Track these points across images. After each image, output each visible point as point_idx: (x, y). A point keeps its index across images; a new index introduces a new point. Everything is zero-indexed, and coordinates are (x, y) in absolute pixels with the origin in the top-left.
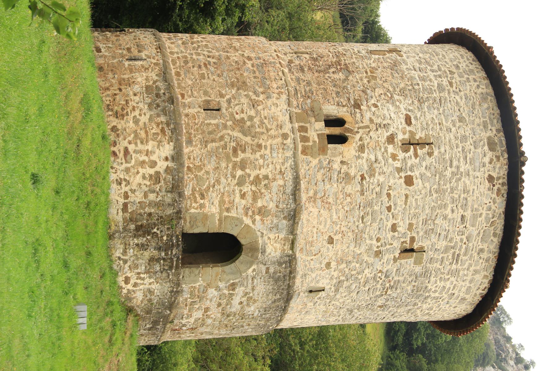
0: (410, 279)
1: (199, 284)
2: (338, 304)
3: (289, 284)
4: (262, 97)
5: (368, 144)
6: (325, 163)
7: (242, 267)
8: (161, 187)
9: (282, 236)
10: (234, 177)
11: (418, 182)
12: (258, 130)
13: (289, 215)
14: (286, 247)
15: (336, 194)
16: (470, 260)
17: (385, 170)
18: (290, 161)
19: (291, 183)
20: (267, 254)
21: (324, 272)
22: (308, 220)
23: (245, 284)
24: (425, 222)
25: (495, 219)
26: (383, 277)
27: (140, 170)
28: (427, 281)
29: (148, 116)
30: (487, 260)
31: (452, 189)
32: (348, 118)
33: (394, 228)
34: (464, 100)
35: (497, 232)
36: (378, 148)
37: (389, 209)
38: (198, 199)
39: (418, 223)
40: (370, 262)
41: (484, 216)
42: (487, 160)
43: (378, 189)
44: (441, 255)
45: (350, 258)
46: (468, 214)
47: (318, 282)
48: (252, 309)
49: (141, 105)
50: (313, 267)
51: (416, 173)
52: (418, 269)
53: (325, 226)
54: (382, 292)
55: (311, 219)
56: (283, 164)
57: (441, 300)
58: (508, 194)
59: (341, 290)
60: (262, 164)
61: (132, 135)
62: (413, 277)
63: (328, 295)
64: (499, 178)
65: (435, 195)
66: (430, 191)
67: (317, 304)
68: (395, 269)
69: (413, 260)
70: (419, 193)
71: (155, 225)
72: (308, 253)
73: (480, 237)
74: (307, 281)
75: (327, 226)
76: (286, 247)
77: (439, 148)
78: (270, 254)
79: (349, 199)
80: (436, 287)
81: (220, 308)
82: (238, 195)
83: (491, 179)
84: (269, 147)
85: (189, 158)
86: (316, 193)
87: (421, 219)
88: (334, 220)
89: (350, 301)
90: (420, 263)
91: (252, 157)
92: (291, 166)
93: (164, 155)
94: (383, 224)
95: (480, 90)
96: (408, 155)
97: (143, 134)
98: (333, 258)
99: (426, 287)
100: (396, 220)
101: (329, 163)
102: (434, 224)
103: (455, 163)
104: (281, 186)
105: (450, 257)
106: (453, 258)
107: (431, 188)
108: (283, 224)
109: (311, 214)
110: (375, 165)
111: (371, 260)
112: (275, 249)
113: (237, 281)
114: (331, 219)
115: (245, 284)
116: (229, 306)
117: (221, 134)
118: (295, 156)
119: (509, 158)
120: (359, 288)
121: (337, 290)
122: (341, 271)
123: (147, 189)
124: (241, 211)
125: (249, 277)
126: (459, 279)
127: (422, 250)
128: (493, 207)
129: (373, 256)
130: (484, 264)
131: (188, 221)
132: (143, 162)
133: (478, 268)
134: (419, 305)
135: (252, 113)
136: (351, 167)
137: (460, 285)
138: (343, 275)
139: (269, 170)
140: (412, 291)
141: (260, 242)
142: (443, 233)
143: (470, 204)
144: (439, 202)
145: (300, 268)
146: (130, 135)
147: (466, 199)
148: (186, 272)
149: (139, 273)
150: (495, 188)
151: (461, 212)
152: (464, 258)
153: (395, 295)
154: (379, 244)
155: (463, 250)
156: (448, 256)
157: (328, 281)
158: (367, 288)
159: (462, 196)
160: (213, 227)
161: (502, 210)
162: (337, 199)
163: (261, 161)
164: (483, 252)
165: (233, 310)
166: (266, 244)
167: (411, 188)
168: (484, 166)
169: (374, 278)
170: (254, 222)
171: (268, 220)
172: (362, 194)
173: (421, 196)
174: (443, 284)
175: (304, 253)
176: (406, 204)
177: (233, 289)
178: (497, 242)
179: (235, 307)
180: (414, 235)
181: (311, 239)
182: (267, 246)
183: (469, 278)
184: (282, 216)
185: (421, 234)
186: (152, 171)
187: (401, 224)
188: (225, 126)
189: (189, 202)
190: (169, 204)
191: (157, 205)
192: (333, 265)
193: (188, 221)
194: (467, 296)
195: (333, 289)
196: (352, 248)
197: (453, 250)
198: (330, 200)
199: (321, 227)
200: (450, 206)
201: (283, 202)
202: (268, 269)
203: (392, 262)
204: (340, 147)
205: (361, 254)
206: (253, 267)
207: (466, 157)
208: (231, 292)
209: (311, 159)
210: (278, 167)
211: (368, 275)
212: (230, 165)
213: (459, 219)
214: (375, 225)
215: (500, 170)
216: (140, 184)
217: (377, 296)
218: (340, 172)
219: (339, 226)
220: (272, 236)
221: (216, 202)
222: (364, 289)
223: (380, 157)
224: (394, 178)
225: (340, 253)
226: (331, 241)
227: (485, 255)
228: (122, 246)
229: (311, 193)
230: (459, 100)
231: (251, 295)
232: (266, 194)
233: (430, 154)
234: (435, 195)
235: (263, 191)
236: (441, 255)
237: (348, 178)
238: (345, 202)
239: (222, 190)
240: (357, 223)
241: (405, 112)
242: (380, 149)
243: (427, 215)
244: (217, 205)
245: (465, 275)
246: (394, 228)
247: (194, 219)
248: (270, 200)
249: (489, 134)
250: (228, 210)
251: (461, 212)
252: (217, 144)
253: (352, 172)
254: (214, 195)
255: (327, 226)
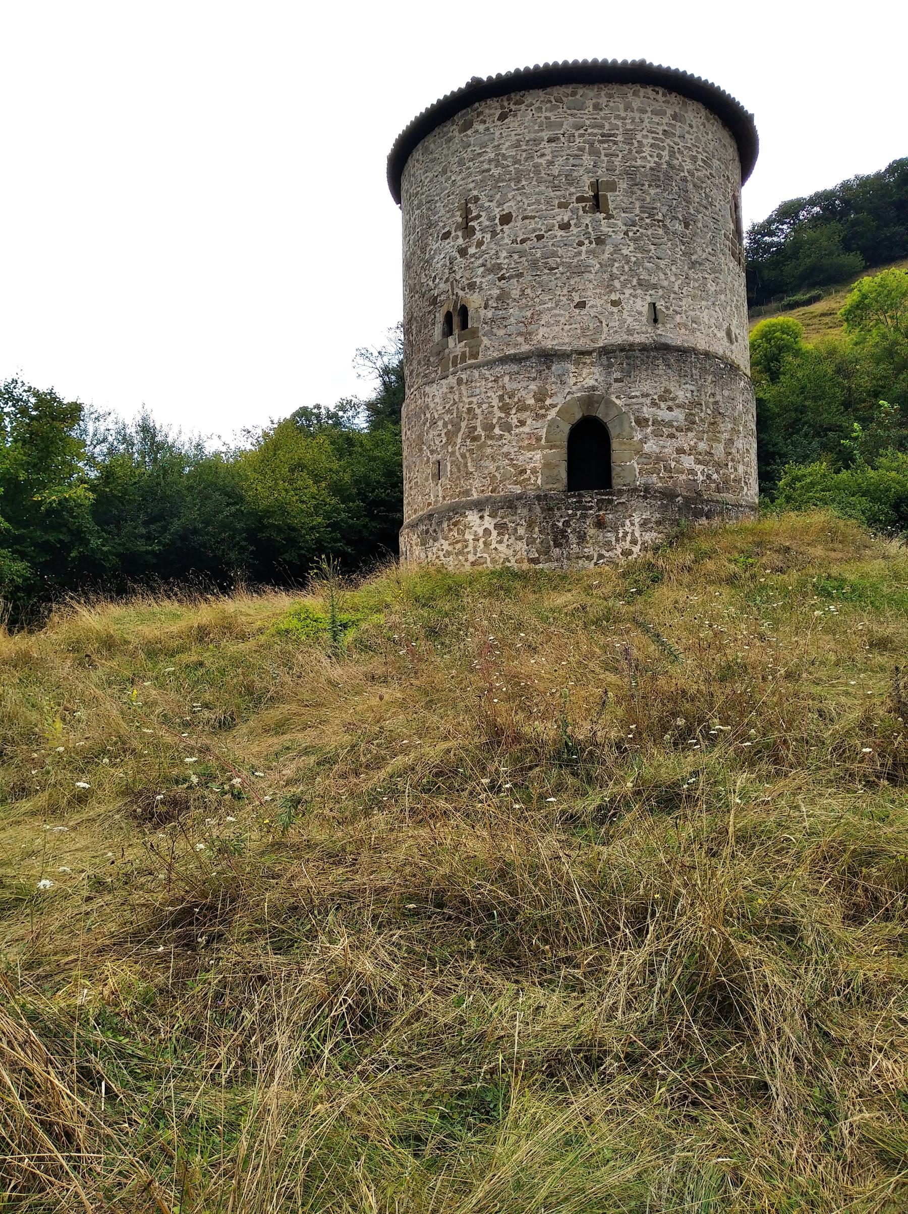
0: (639, 192)
1: (635, 465)
2: (680, 281)
3: (640, 350)
4: (428, 415)
5: (468, 279)
6: (487, 328)
7: (613, 412)
8: (510, 522)
9: (572, 368)
10: (501, 436)
11: (508, 207)
12: (455, 415)
13: (545, 363)
14: (588, 361)
15: (521, 309)
16: (609, 118)
17: (494, 252)
18: (483, 371)
19: (507, 366)
20: (596, 384)
21: (625, 306)
22: (554, 338)
23: (636, 407)
24: (556, 188)
25: (552, 99)
26: (635, 229)
27: (492, 547)
28: (643, 170)
29: (443, 541)
30: (611, 96)
31: (515, 163)
32: (444, 310)
33: (565, 227)
34: (428, 174)
35: (569, 93)
36: (471, 266)
37: (540, 238)
38: (526, 476)
39: (558, 197)
40: (612, 249)
41: (548, 114)
42: (481, 128)
43: (516, 256)
44: (603, 157)
45: (606, 276)
46: (546, 135)
47: (640, 313)
48: (682, 394)
49: (435, 549)
50: (617, 323)
51: (497, 212)
52: (623, 185)
53: (561, 315)
54: (659, 226)
55: (549, 336)
56: (487, 379)
57: (676, 147)
58: (520, 91)
59: (654, 281)
60: (487, 405)
61: (460, 557)
62: (635, 188)
63: (662, 297)
64: (502, 107)
65: (524, 183)
66: (518, 189)
67: (678, 309)
68: (623, 215)
69: (609, 194)
70: (521, 204)
71: (554, 525)
72: (598, 330)
73: (576, 111)
74: (637, 327)
75: (562, 312)
76: (588, 361)
77: (471, 190)
78: (596, 380)
79: (528, 291)
80: (651, 156)
81: (678, 434)
82: (521, 429)
83: (503, 117)
84: (470, 399)
85: (483, 491)
86: (520, 334)
87: (552, 194)
88: (554, 305)
89: (673, 268)
90: (614, 183)
91: (480, 418)
92: (489, 370)
93: (478, 521)
94: (559, 241)
95: (421, 158)
96: (478, 228)
97: (459, 546)
98: (606, 298)
99: (651, 169)
100: (554, 226)
101: (486, 323)
102: (559, 175)
103: (486, 166)
104: (511, 378)
105: (606, 146)
106: (607, 141)
107: (514, 190)
108: (557, 370)
109: (546, 335)
110: (489, 266)
111: (609, 249)
112: (590, 374)
113: (632, 417)
114: (552, 308)
115: (636, 407)
116: (675, 424)
117: (459, 456)
118: (477, 367)
119: (479, 101)
120: (651, 257)
121: (655, 287)
122: (624, 286)
123: (513, 537)
124: (539, 424)
125: (628, 403)
126: (640, 128)
127: (595, 186)
128: (538, 105)
129: (603, 247)
130: (617, 100)
131: (551, 486)
132: (485, 543)
133: (621, 106)
134: (686, 174)
135: (440, 423)
136: (490, 294)
137: (648, 125)
138: (630, 282)
139: (493, 396)
140: (658, 186)
141: (579, 395)
142: (572, 161)
143: (533, 136)
144: (532, 175)
145: (620, 339)
146: (460, 561)
147: (528, 141)
148: (617, 482)
149: (617, 540)
150: (513, 107)
151: (544, 144)
152: (607, 126)
153: (665, 209)
154: (587, 242)
155: (596, 131)
156: (604, 149)
157: (639, 301)
158: (652, 247)
159: (524, 147)
160: (559, 455)
161: (541, 93)
162: (527, 306)
163: (485, 406)
164: (598, 103)
165: (682, 417)
166: (583, 386)
167: (514, 215)
168: (487, 129)
169: (635, 240)
170: (554, 406)
171: (551, 388)
172: (520, 275)
173: (524, 200)
174: (647, 150)
175: (598, 336)
176: (533, 217)
177: (647, 420)
178: (584, 89)
179: (679, 415)
180: (574, 197)
181: (579, 331)
182: (586, 386)
183: (637, 115)
184: (547, 371)
185: (573, 190)
186: (494, 533)
187: (559, 218)
188: (453, 453)
189: (529, 487)
190: (530, 510)
191: (530, 526)
192: (614, 297)
193: (551, 486)
194: (669, 112)
195: (652, 292)
196: (592, 276)
197: (596, 143)
198: (529, 314)
199: (563, 320)
200: (537, 160)
201: (529, 372)
202: (616, 380)
203: (612, 221)
204: (471, 313)
205: (600, 263)
206: (614, 399)
207: (479, 154)
208: (650, 423)
209: (482, 346)
210: (490, 385)
211: (631, 249)
212: (490, 442)
213: (553, 144)
214: (560, 252)
215: (492, 108)
216: (508, 545)
217: (665, 232)
218: (496, 308)
219: (561, 298)
220: (572, 381)
221: (529, 455)
222: (653, 251)
223: (481, 261)
224: (503, 238)
225: (598, 291)
226: (581, 305)
227: (603, 101)
228: (581, 562)
229: (520, 339)
230: (428, 179)
231: (656, 397)
232: (519, 395)
233: (477, 199)
234: (524, 183)
235: (516, 400)
236: (603, 157)
237: (503, 297)
238: (531, 295)
239: (516, 449)
240: (558, 275)
241: (440, 242)
242: (472, 263)
243: (547, 187)
244: (533, 453)
245: (633, 121)
246: (565, 227)
247: (548, 479)
248: (527, 392)
249: (456, 133)
250: (539, 439)
251: (544, 144)
252: (469, 460)
253: (496, 292)
254: (521, 458)
255: (562, 312)
